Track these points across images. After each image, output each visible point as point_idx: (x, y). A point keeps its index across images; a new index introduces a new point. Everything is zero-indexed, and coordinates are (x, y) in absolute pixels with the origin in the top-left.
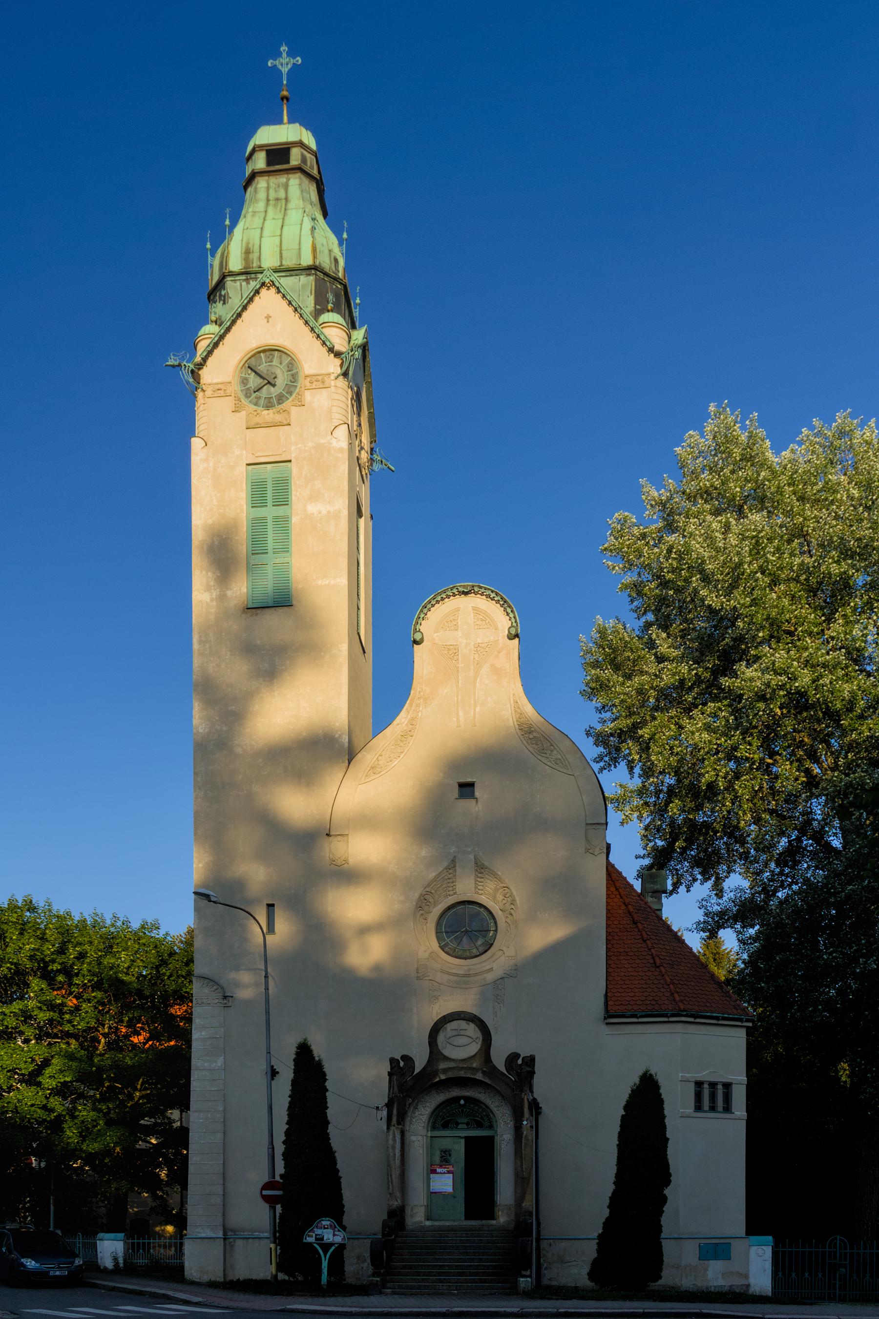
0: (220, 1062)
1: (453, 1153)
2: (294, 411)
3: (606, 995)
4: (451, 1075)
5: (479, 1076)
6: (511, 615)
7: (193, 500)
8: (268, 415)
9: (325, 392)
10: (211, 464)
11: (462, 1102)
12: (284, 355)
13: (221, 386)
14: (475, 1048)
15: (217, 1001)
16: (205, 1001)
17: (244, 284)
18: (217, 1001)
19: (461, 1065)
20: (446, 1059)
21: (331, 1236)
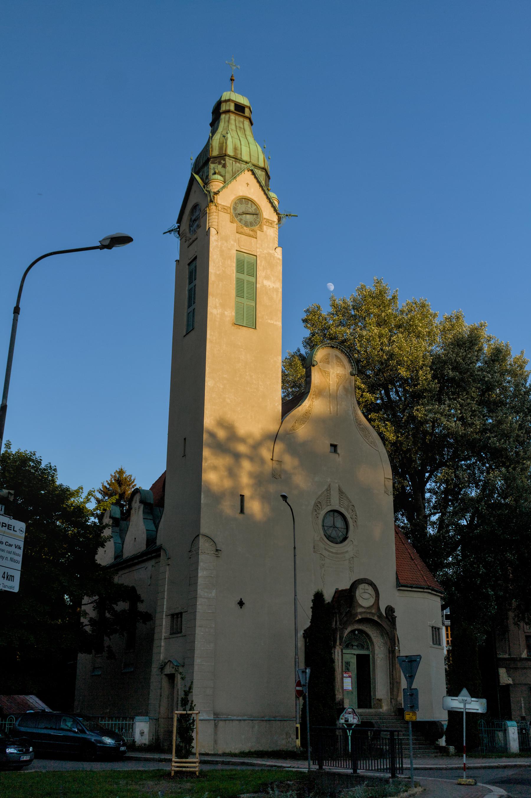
0: (213, 594)
1: (351, 664)
2: (259, 232)
3: (397, 574)
4: (364, 616)
5: (376, 618)
6: (353, 364)
7: (210, 259)
8: (247, 230)
9: (272, 229)
10: (220, 244)
11: (357, 632)
12: (253, 204)
13: (226, 208)
14: (372, 601)
15: (212, 552)
16: (206, 551)
17: (234, 163)
18: (212, 552)
19: (368, 611)
20: (361, 606)
21: (352, 719)
